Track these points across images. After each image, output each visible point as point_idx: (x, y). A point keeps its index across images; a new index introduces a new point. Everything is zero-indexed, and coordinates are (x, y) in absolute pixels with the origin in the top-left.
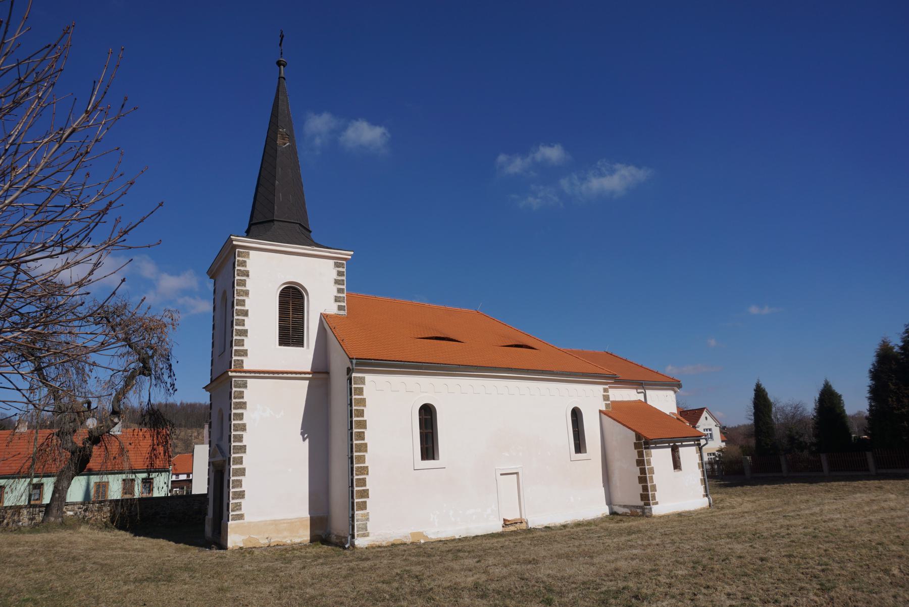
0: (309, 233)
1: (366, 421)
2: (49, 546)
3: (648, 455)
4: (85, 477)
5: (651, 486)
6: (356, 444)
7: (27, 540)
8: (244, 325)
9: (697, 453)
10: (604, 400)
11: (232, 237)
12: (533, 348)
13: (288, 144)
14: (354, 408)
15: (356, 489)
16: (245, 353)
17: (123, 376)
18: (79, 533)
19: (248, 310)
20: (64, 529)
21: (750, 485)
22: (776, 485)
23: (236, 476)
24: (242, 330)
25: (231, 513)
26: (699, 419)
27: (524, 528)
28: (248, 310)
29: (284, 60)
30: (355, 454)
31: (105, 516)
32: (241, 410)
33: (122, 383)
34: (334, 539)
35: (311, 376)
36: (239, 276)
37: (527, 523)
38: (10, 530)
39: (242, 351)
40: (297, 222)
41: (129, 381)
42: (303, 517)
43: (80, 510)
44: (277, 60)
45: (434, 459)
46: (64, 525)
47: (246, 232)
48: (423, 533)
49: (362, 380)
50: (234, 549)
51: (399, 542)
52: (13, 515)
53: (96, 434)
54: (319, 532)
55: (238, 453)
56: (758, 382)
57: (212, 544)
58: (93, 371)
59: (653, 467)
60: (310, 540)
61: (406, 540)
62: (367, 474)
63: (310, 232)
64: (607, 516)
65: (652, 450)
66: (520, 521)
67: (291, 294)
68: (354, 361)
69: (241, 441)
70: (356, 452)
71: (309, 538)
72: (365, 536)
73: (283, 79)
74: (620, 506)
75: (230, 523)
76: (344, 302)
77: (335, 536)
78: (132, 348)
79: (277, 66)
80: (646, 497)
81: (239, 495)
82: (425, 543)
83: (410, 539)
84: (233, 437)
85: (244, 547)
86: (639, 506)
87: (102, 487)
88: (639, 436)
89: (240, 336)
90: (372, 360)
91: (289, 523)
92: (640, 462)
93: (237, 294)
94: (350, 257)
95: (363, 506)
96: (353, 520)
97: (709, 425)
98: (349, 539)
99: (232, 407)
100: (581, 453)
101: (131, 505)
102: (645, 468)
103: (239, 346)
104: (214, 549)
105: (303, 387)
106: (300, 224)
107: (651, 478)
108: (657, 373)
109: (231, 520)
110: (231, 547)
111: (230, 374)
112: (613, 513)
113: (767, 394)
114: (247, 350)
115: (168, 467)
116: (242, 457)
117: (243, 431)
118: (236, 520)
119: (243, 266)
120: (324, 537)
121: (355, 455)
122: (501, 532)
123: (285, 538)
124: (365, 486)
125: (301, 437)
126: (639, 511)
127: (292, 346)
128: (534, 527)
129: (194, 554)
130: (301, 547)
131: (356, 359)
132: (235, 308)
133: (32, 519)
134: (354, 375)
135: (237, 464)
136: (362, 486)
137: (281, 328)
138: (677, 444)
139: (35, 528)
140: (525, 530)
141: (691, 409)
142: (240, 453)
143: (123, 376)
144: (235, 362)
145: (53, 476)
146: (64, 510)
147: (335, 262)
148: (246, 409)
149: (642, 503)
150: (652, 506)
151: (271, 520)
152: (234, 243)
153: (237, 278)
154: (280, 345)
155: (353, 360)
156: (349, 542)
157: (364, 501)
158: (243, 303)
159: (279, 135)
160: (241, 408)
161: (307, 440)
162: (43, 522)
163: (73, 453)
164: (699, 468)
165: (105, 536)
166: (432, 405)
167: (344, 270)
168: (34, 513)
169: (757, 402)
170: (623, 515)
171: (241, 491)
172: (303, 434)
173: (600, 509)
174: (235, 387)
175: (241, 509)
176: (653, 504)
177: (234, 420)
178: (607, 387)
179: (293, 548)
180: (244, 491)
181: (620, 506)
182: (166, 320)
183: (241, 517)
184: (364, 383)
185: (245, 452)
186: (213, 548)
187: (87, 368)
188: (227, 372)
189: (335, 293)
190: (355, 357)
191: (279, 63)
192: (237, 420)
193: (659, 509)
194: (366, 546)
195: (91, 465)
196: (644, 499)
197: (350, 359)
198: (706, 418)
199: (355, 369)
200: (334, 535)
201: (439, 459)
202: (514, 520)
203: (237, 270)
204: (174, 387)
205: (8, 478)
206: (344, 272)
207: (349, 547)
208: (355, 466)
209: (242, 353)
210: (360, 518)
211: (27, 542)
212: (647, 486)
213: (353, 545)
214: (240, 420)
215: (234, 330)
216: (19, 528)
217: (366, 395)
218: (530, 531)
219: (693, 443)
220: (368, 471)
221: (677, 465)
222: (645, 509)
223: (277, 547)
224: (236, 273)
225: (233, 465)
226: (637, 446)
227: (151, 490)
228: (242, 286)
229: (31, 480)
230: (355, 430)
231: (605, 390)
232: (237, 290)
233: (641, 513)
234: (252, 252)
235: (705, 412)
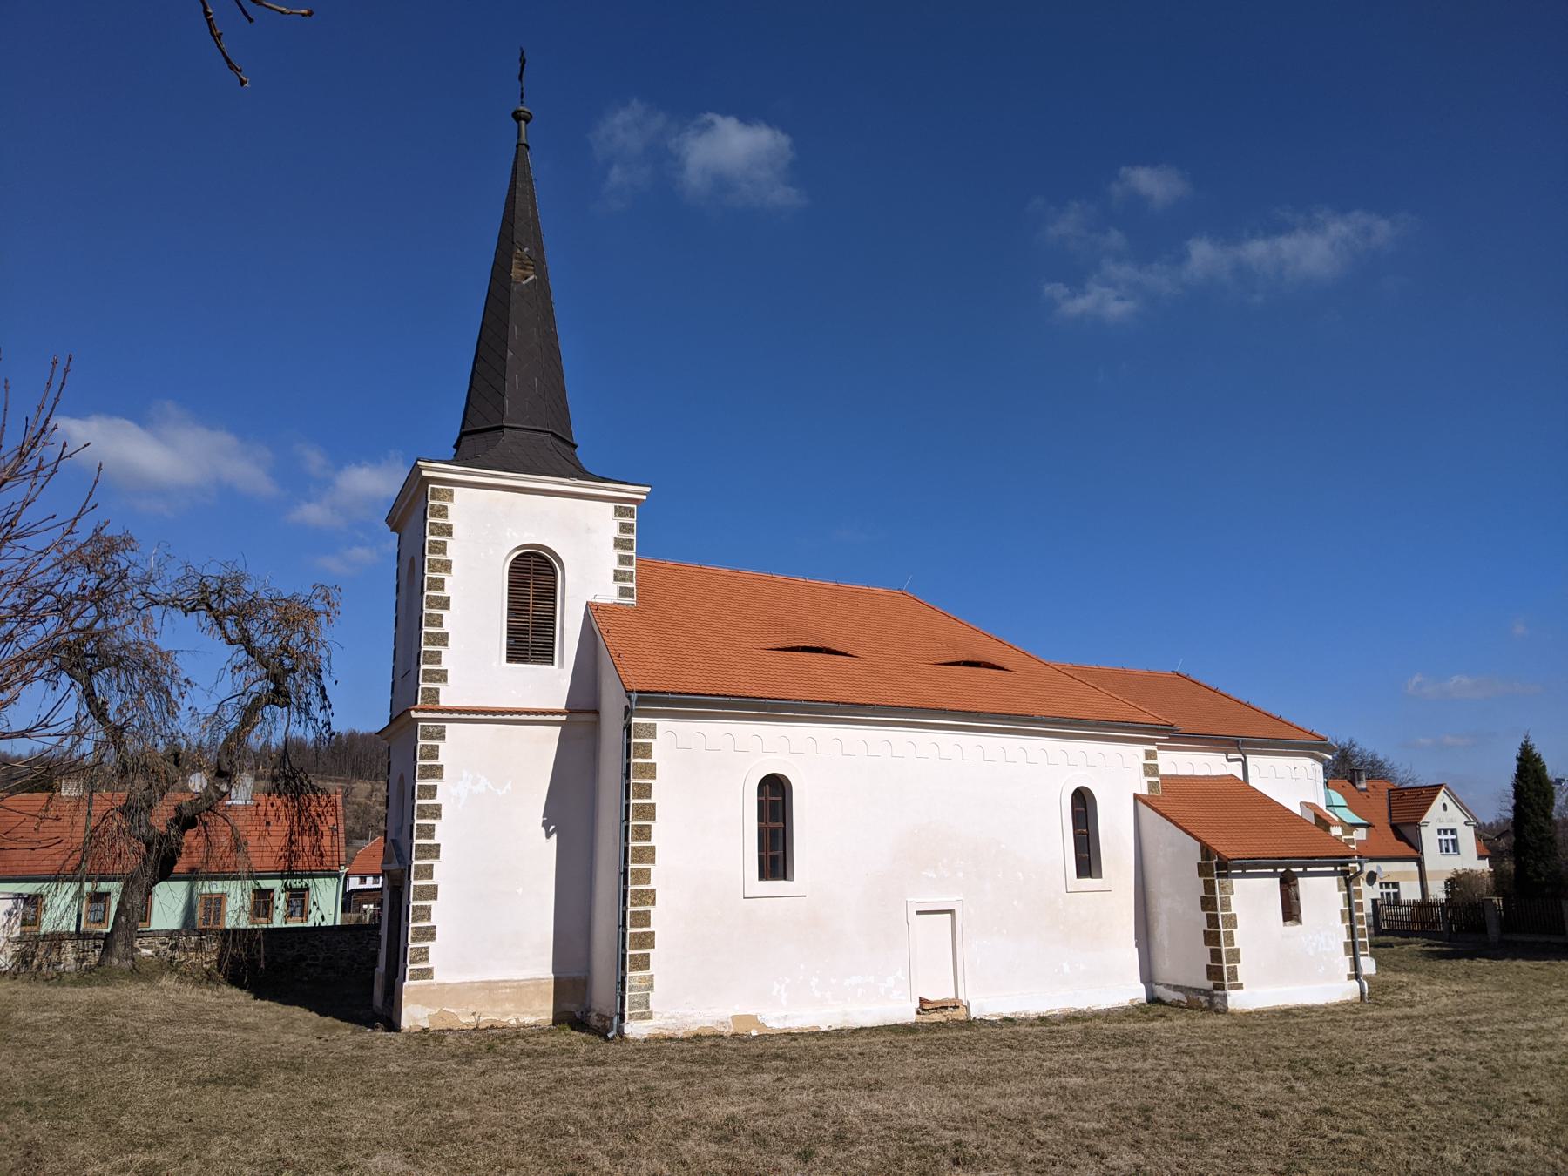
0: (572, 449)
1: (654, 805)
2: (102, 1008)
3: (1223, 889)
4: (184, 884)
5: (1228, 951)
6: (633, 848)
7: (64, 999)
8: (441, 625)
9: (1339, 890)
10: (1146, 774)
11: (419, 463)
12: (1002, 669)
13: (532, 278)
14: (633, 781)
15: (630, 930)
16: (442, 676)
17: (239, 706)
18: (158, 988)
19: (449, 597)
20: (134, 979)
21: (1488, 958)
22: (1542, 963)
23: (420, 900)
24: (438, 633)
25: (410, 967)
26: (1428, 808)
27: (962, 1018)
28: (449, 597)
29: (526, 110)
30: (631, 866)
31: (208, 960)
32: (433, 780)
33: (237, 719)
34: (594, 1020)
35: (564, 718)
36: (433, 534)
37: (967, 1008)
38: (44, 977)
40: (547, 429)
41: (249, 715)
42: (542, 977)
43: (165, 947)
44: (512, 111)
45: (785, 878)
46: (139, 972)
47: (454, 447)
48: (756, 1016)
49: (651, 731)
50: (414, 1031)
51: (708, 1032)
52: (50, 950)
53: (187, 812)
54: (571, 1007)
55: (425, 858)
56: (1526, 742)
57: (375, 1022)
58: (186, 696)
59: (1235, 915)
60: (553, 1020)
61: (722, 1029)
62: (653, 903)
63: (575, 446)
64: (1139, 1007)
65: (1234, 880)
66: (953, 1005)
67: (532, 567)
68: (634, 696)
69: (432, 837)
70: (633, 862)
71: (551, 1017)
72: (644, 1019)
73: (524, 147)
74: (1168, 986)
75: (407, 983)
76: (632, 581)
77: (597, 1015)
78: (253, 656)
79: (514, 121)
80: (1219, 972)
82: (759, 1036)
83: (730, 1027)
84: (417, 829)
85: (432, 1029)
86: (1204, 990)
87: (216, 904)
88: (1207, 852)
89: (434, 645)
90: (668, 693)
91: (514, 987)
92: (1208, 903)
93: (429, 567)
94: (644, 497)
95: (643, 963)
96: (623, 989)
97: (1451, 821)
98: (615, 1023)
99: (417, 774)
100: (1091, 877)
101: (251, 941)
102: (1217, 915)
103: (432, 663)
104: (380, 1029)
105: (550, 736)
106: (552, 433)
107: (1230, 936)
108: (1278, 719)
109: (410, 979)
110: (407, 1027)
111: (414, 714)
112: (1154, 1000)
113: (1544, 767)
114: (446, 671)
115: (337, 868)
116: (432, 865)
117: (435, 818)
118: (418, 979)
119: (441, 516)
120: (578, 1015)
121: (632, 869)
122: (912, 1024)
123: (507, 1014)
124: (649, 925)
125: (543, 830)
126: (1202, 998)
127: (532, 663)
128: (983, 1017)
129: (346, 1037)
130: (536, 1031)
131: (638, 692)
132: (426, 594)
133: (79, 960)
134: (635, 720)
135: (422, 877)
136: (642, 926)
137: (512, 631)
138: (1293, 870)
139: (86, 976)
140: (961, 1022)
141: (1424, 784)
142: (429, 859)
143: (239, 706)
144: (423, 693)
145: (119, 880)
146: (137, 944)
147: (615, 507)
148: (441, 778)
149: (1209, 985)
150: (1228, 991)
151: (482, 982)
152: (425, 473)
153: (430, 538)
154: (508, 661)
155: (632, 695)
156: (615, 1027)
157: (644, 954)
158: (441, 585)
159: (515, 261)
160: (433, 776)
161: (554, 837)
162: (99, 964)
163: (149, 846)
164: (1343, 921)
165: (201, 997)
167: (633, 521)
168: (86, 949)
169: (1521, 783)
170: (1172, 1006)
171: (429, 927)
172: (546, 825)
173: (1135, 992)
174: (423, 738)
175: (427, 959)
176: (1231, 987)
177: (419, 798)
178: (1153, 748)
179: (519, 1033)
180: (435, 927)
181: (1168, 986)
182: (318, 605)
183: (427, 973)
184: (654, 736)
185: (437, 857)
186: (377, 1027)
187: (174, 692)
188: (409, 710)
189: (615, 564)
190: (635, 688)
191: (517, 116)
192: (425, 798)
193: (1238, 1000)
194: (646, 1037)
195: (177, 869)
196: (1213, 976)
197: (627, 691)
198: (1445, 806)
199: (636, 710)
200: (594, 1014)
201: (793, 880)
202: (941, 1002)
203: (430, 523)
204: (330, 729)
205: (44, 881)
206: (633, 525)
207: (613, 1037)
208: (631, 888)
209: (437, 677)
210: (636, 984)
211: (63, 1003)
212: (1220, 951)
213: (621, 1033)
215: (423, 635)
216: (60, 974)
217: (656, 758)
218: (971, 1024)
219: (1332, 869)
220: (655, 898)
221: (1291, 912)
222: (1214, 995)
223: (490, 1031)
224: (428, 529)
225: (415, 879)
226: (1203, 870)
227: (304, 913)
229: (81, 887)
230: (632, 823)
231: (1150, 755)
232: (429, 560)
233: (1206, 1005)
234: (457, 490)
235: (1441, 793)
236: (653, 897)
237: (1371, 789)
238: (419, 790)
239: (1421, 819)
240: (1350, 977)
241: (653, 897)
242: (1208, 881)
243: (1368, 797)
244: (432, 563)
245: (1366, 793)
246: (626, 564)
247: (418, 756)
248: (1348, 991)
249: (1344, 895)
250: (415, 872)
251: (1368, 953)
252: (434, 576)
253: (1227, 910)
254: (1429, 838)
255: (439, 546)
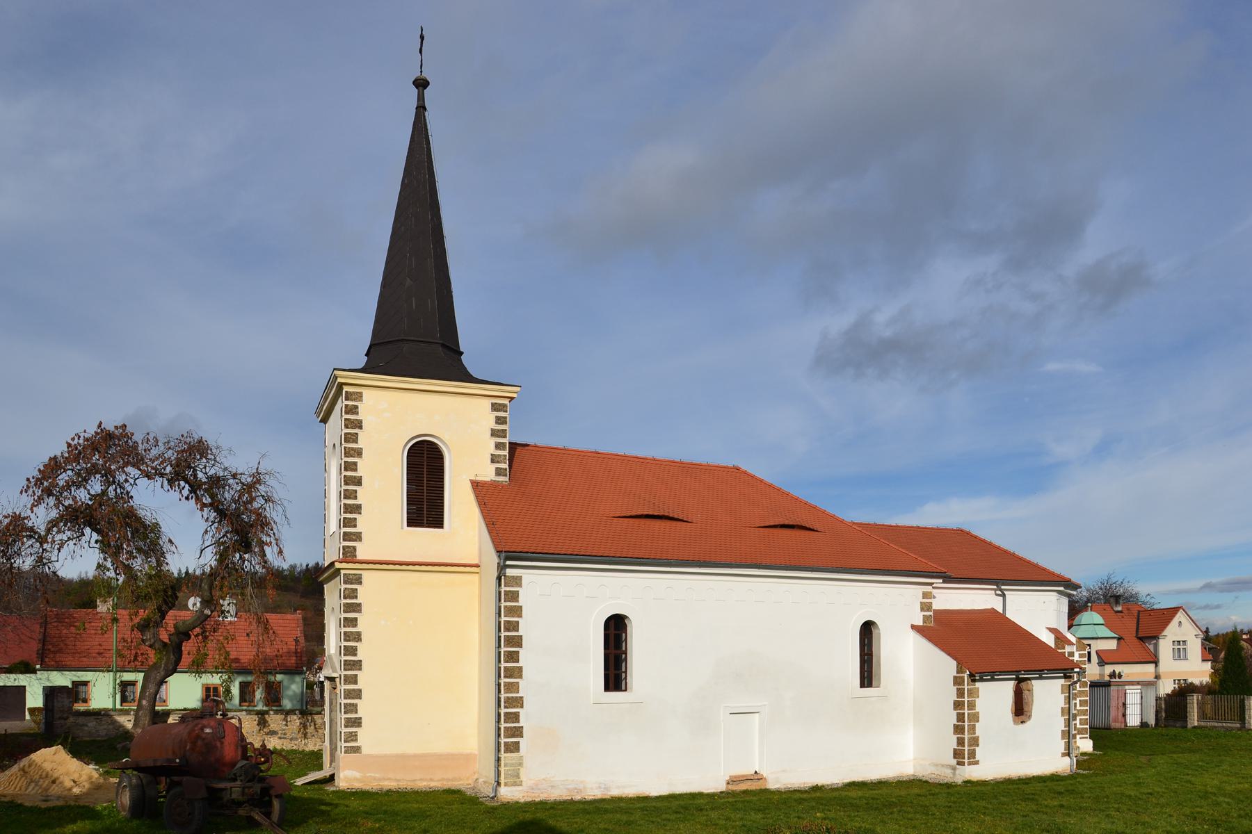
8: (356, 498)
23: (349, 698)
24: (354, 505)
26: (1167, 625)
36: (347, 428)
39: (354, 534)
47: (366, 355)
62: (522, 707)
81: (354, 722)
99: (342, 609)
117: (357, 642)
154: (408, 526)
157: (516, 742)
160: (354, 611)
164: (1063, 715)
166: (616, 614)
176: (969, 764)
180: (361, 718)
185: (360, 669)
212: (964, 739)
214: (353, 627)
221: (1020, 709)
228: (352, 442)
234: (365, 392)
236: (521, 702)
237: (1125, 611)
238: (344, 621)
239: (1160, 633)
240: (1064, 755)
241: (521, 702)
242: (960, 689)
243: (1123, 617)
244: (347, 450)
245: (1121, 614)
246: (500, 449)
247: (342, 596)
248: (1061, 765)
249: (1065, 697)
250: (344, 680)
251: (1088, 736)
252: (349, 461)
253: (972, 709)
254: (1165, 647)
255: (352, 437)
